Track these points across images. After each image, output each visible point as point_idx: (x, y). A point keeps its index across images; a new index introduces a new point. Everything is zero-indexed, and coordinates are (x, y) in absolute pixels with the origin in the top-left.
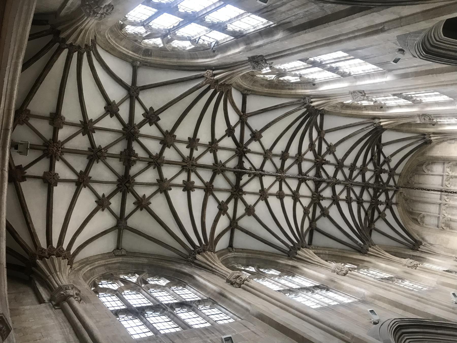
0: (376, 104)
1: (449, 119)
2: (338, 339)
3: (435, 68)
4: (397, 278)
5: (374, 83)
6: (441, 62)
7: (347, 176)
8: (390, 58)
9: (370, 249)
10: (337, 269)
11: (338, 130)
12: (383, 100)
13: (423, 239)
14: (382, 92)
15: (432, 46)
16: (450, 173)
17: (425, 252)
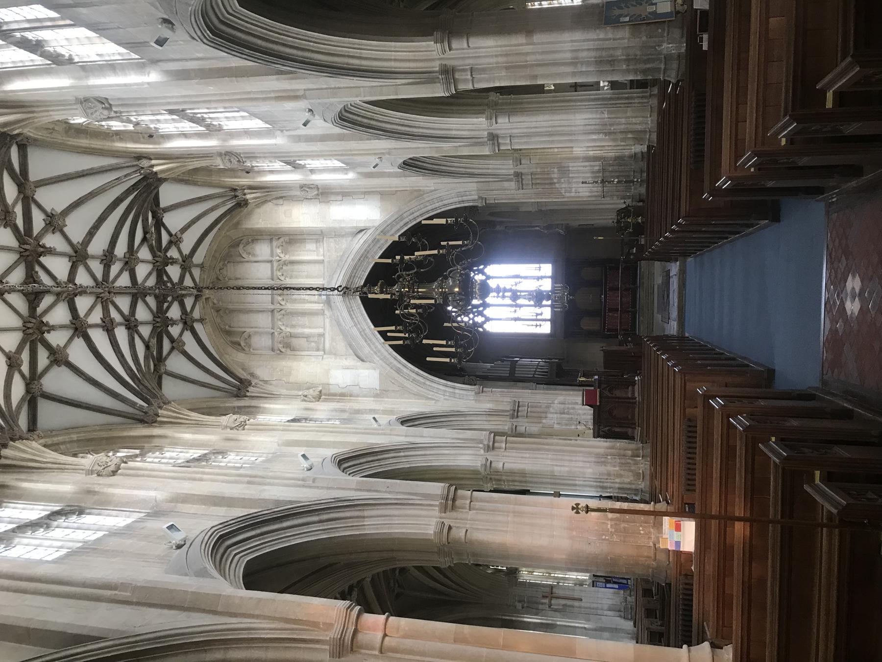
0: (138, 128)
1: (271, 162)
2: (104, 604)
3: (234, 65)
4: (214, 453)
5: (125, 85)
6: (249, 58)
7: (99, 276)
8: (149, 34)
9: (160, 412)
10: (97, 467)
11: (64, 180)
12: (152, 121)
13: (252, 375)
14: (145, 105)
15: (221, 22)
16: (282, 256)
17: (258, 397)
